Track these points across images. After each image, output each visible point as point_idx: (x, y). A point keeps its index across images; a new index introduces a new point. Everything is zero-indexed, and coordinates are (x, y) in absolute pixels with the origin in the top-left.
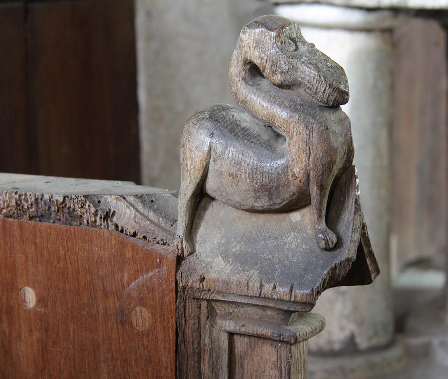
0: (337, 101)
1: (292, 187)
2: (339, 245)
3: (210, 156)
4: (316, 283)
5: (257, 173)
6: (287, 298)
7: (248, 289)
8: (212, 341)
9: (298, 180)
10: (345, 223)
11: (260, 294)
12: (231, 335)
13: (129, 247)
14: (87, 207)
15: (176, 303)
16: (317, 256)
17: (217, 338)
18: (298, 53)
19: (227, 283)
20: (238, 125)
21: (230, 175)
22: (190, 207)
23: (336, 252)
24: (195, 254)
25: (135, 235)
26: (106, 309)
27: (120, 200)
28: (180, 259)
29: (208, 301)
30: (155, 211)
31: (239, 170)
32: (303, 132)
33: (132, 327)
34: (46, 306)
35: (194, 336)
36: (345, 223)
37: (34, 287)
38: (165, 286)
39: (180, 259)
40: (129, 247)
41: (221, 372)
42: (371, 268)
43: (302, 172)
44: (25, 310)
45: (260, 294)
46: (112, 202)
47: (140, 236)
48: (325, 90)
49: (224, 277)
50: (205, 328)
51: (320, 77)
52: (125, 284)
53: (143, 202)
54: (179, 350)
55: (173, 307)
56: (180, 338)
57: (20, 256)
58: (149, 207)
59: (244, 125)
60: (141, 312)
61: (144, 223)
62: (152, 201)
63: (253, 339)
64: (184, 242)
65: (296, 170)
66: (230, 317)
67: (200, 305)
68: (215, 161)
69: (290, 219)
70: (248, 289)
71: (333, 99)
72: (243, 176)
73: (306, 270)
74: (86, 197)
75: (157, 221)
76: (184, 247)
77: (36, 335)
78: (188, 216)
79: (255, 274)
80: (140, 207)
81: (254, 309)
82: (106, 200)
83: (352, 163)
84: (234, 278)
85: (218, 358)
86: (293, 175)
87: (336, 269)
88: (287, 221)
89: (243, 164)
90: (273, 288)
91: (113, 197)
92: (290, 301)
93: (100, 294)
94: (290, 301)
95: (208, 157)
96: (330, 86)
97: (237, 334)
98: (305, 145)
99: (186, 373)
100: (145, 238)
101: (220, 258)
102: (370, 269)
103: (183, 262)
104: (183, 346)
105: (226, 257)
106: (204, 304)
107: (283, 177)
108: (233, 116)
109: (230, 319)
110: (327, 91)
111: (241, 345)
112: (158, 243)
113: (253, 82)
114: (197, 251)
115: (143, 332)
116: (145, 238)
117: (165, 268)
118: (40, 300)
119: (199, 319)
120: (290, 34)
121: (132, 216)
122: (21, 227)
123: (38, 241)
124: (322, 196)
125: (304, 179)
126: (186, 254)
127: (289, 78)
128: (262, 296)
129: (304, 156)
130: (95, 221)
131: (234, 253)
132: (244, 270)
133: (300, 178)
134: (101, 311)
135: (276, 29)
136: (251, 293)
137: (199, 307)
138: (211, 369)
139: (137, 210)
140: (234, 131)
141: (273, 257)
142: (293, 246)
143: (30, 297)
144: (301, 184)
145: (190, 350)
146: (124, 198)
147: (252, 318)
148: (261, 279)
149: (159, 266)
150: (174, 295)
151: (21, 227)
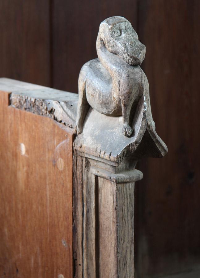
0: (133, 63)
1: (114, 104)
2: (133, 135)
3: (86, 85)
4: (119, 152)
5: (101, 96)
6: (108, 158)
7: (96, 153)
8: (88, 178)
9: (116, 101)
10: (138, 124)
11: (100, 155)
12: (97, 177)
13: (57, 127)
14: (43, 105)
15: (73, 157)
16: (124, 139)
17: (90, 177)
18: (120, 37)
19: (89, 149)
20: (99, 71)
21: (92, 95)
22: (82, 110)
23: (131, 138)
24: (82, 134)
25: (61, 122)
26: (49, 158)
27: (57, 104)
28: (75, 136)
29: (86, 158)
30: (71, 110)
31: (95, 93)
32: (117, 77)
33: (58, 168)
34: (28, 154)
35: (80, 175)
36: (138, 124)
37: (25, 144)
38: (68, 149)
39: (75, 136)
40: (57, 127)
41: (92, 194)
42: (160, 149)
43: (117, 97)
44: (22, 155)
45: (100, 155)
46: (54, 105)
47: (63, 122)
48: (127, 57)
49: (88, 146)
50: (84, 172)
51: (125, 51)
52: (55, 146)
53: (67, 105)
54: (74, 181)
55: (72, 160)
56: (75, 176)
57: (20, 128)
58: (69, 108)
59: (102, 70)
60: (61, 160)
61: (65, 116)
62: (72, 106)
63: (104, 179)
64: (77, 127)
65: (115, 96)
66: (95, 167)
67: (83, 160)
68: (87, 88)
69: (118, 120)
70: (96, 153)
71: (131, 62)
72: (96, 96)
73: (118, 146)
74: (43, 100)
75: (71, 116)
76: (77, 129)
77: (25, 169)
78: (80, 115)
79: (99, 146)
80: (65, 107)
81: (103, 164)
82: (52, 103)
83: (143, 94)
84: (94, 147)
85: (91, 187)
86: (114, 98)
87: (130, 147)
88: (117, 121)
89: (96, 90)
90: (104, 153)
91: (55, 102)
92: (109, 160)
93: (47, 150)
94: (109, 160)
95: (85, 85)
96: (129, 55)
97: (99, 176)
98: (118, 83)
99: (77, 193)
100: (65, 124)
101: (90, 136)
102: (160, 149)
103: (76, 137)
104: (75, 179)
105: (92, 136)
106: (84, 159)
107: (110, 98)
108: (99, 66)
109: (95, 168)
110: (128, 58)
111: (100, 181)
112: (69, 127)
113: (104, 50)
114: (83, 132)
115: (61, 171)
116: (65, 124)
117: (69, 139)
118: (27, 151)
119: (82, 167)
120: (119, 27)
121: (61, 112)
122: (20, 113)
123: (26, 121)
124: (126, 110)
125: (118, 101)
126: (78, 134)
127: (114, 50)
128: (100, 157)
129: (117, 89)
130: (46, 113)
131: (95, 135)
132: (96, 143)
133: (116, 100)
134: (47, 159)
135: (111, 24)
136: (97, 155)
137: (82, 161)
138: (87, 193)
139: (63, 109)
140: (96, 74)
141: (109, 138)
142: (117, 134)
143: (23, 148)
144: (118, 103)
145: (79, 182)
146: (59, 103)
147: (103, 169)
148: (101, 148)
149: (66, 138)
150: (72, 154)
151: (20, 113)
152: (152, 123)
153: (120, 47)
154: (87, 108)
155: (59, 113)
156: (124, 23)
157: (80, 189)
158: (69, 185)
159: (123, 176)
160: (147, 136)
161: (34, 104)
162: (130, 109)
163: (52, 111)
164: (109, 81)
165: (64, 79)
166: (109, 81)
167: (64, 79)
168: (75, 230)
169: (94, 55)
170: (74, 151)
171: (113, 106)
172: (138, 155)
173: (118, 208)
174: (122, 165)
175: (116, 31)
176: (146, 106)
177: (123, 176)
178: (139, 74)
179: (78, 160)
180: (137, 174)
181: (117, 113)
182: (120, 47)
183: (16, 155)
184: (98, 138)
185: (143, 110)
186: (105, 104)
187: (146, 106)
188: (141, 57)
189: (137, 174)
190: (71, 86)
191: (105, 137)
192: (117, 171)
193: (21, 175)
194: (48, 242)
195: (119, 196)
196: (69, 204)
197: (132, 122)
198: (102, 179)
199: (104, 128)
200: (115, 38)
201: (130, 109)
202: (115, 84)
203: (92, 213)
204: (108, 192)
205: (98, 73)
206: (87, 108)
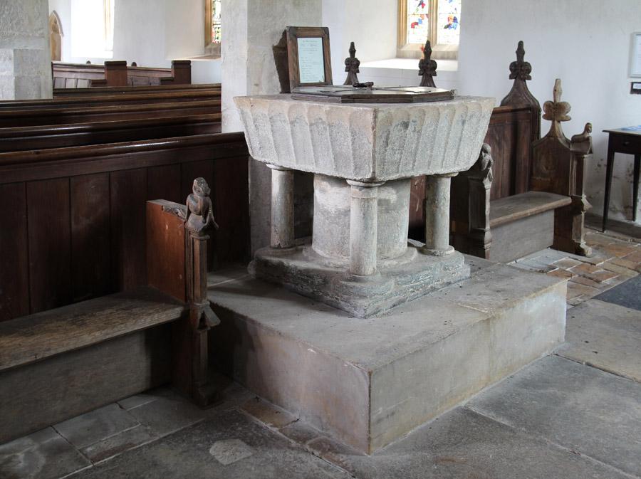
2: (205, 222)
37: (211, 183)
46: (178, 210)
152: (213, 218)
153: (201, 189)
154: (189, 212)
155: (180, 213)
156: (203, 180)
157: (187, 243)
158: (183, 241)
159: (203, 238)
160: (211, 222)
161: (170, 210)
162: (204, 212)
163: (177, 213)
164: (197, 202)
165: (183, 201)
166: (197, 202)
167: (183, 201)
168: (185, 258)
169: (192, 192)
170: (185, 229)
171: (199, 211)
172: (205, 231)
173: (201, 250)
174: (202, 233)
175: (199, 183)
176: (211, 211)
177: (203, 238)
178: (208, 199)
179: (186, 231)
180: (208, 237)
181: (200, 214)
182: (201, 189)
183: (164, 229)
184: (193, 224)
185: (210, 213)
186: (196, 211)
187: (211, 211)
188: (209, 193)
189: (208, 237)
190: (183, 202)
191: (195, 223)
192: (200, 236)
193: (166, 237)
194: (483, 280)
195: (201, 245)
196: (183, 248)
197: (205, 217)
198: (325, 184)
199: (196, 220)
200: (199, 186)
201: (204, 212)
202: (199, 204)
203: (562, 201)
204: (197, 243)
205: (193, 199)
206: (189, 212)
